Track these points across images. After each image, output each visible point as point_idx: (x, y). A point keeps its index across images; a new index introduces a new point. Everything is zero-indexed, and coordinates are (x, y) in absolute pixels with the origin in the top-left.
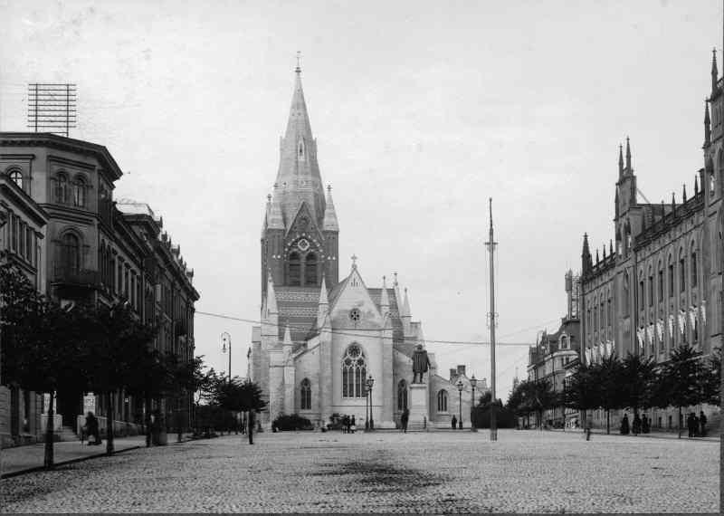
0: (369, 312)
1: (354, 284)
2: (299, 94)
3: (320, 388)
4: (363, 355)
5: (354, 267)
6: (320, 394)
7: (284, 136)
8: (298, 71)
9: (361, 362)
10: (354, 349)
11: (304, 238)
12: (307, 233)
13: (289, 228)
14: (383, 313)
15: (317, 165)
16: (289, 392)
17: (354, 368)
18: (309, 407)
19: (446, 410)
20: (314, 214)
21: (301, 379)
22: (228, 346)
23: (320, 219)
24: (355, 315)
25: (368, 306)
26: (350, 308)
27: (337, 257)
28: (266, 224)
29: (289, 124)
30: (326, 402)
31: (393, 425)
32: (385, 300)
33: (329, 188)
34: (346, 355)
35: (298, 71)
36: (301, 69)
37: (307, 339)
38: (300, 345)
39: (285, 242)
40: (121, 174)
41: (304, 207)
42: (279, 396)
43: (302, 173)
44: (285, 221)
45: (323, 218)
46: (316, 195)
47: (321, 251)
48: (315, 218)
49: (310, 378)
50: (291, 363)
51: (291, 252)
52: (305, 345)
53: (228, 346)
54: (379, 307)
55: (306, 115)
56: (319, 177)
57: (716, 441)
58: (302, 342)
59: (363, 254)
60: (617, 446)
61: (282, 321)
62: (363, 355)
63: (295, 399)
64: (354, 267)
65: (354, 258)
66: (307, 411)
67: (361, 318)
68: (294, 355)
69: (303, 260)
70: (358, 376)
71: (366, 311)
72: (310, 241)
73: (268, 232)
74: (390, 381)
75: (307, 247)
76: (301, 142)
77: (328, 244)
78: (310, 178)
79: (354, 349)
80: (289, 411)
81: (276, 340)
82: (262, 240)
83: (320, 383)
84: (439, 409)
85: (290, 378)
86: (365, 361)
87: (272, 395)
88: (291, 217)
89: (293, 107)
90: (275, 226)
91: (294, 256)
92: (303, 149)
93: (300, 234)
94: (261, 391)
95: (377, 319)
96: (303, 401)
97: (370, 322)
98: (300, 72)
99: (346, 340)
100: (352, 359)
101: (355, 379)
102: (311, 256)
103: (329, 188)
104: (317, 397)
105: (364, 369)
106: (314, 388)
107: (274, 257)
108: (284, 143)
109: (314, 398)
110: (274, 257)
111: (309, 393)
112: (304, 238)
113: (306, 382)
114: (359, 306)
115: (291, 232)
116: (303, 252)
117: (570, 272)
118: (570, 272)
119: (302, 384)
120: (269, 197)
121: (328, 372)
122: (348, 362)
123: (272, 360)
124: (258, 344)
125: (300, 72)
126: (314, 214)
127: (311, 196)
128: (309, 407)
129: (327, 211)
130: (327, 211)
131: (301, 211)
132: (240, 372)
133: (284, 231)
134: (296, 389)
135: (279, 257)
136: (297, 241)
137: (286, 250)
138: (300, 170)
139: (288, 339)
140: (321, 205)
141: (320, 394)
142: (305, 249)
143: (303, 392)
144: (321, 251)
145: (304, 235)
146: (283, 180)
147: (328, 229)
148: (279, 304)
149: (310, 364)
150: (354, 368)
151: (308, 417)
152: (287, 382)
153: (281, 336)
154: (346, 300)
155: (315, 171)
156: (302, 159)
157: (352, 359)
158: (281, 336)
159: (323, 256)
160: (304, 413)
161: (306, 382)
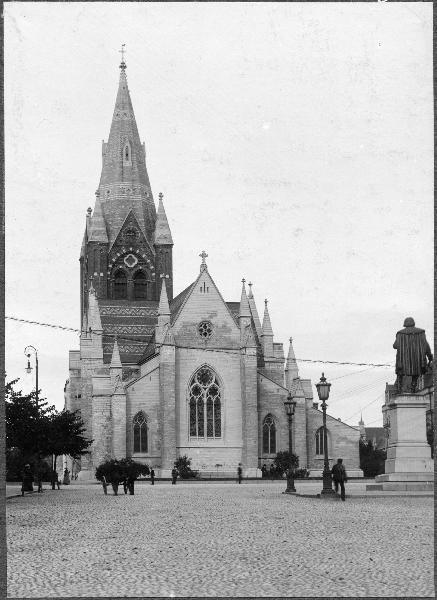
0: (224, 326)
1: (204, 289)
2: (124, 91)
3: (161, 424)
4: (216, 382)
5: (204, 268)
6: (160, 432)
7: (106, 141)
8: (123, 66)
9: (213, 391)
10: (204, 375)
11: (130, 252)
12: (135, 247)
13: (113, 241)
14: (243, 327)
15: (146, 171)
16: (120, 430)
17: (205, 400)
18: (145, 449)
20: (143, 226)
21: (134, 412)
22: (33, 365)
23: (151, 231)
24: (205, 329)
25: (223, 318)
26: (199, 320)
27: (171, 274)
28: (86, 238)
29: (113, 127)
30: (168, 444)
31: (361, 473)
32: (244, 312)
33: (161, 196)
34: (193, 382)
35: (123, 66)
36: (126, 64)
37: (140, 363)
38: (132, 371)
41: (131, 218)
42: (106, 436)
43: (128, 180)
44: (108, 233)
45: (154, 230)
46: (146, 211)
48: (143, 230)
49: (93, 472)
50: (121, 391)
51: (116, 269)
52: (137, 371)
53: (33, 365)
54: (238, 321)
55: (132, 116)
56: (149, 185)
57: (428, 496)
58: (136, 367)
59: (204, 246)
60: (207, 489)
61: (107, 339)
62: (216, 382)
63: (127, 440)
64: (204, 268)
65: (204, 255)
66: (141, 455)
67: (214, 331)
68: (124, 383)
69: (130, 281)
70: (209, 409)
71: (220, 325)
72: (139, 256)
73: (89, 245)
74: (253, 415)
75: (134, 264)
76: (128, 144)
77: (157, 259)
78: (138, 186)
79: (204, 375)
80: (119, 455)
81: (100, 364)
82: (81, 260)
83: (160, 417)
86: (220, 390)
87: (94, 428)
88: (116, 229)
89: (117, 106)
90: (97, 238)
91: (120, 274)
92: (130, 152)
93: (127, 247)
94: (80, 425)
95: (235, 334)
96: (137, 440)
97: (225, 339)
98: (125, 67)
99: (195, 360)
100: (201, 386)
102: (140, 274)
103: (161, 196)
105: (218, 400)
106: (153, 425)
107: (96, 274)
108: (107, 149)
109: (153, 440)
110: (96, 274)
111: (145, 430)
112: (130, 252)
113: (141, 416)
114: (211, 317)
115: (115, 245)
117: (409, 323)
118: (409, 323)
119: (135, 419)
120: (90, 210)
121: (170, 405)
122: (196, 391)
124: (75, 371)
125: (125, 67)
126: (143, 226)
127: (139, 206)
128: (145, 449)
129: (158, 223)
130: (158, 222)
131: (127, 222)
132: (54, 400)
133: (108, 245)
134: (128, 426)
135: (102, 274)
136: (123, 256)
137: (110, 266)
138: (125, 176)
139: (116, 359)
140: (152, 218)
141: (160, 432)
143: (136, 431)
148: (105, 320)
149: (146, 392)
150: (205, 400)
151: (143, 462)
152: (116, 416)
153: (107, 359)
154: (191, 314)
155: (144, 179)
156: (127, 164)
157: (201, 386)
158: (107, 359)
160: (139, 458)
161: (141, 416)
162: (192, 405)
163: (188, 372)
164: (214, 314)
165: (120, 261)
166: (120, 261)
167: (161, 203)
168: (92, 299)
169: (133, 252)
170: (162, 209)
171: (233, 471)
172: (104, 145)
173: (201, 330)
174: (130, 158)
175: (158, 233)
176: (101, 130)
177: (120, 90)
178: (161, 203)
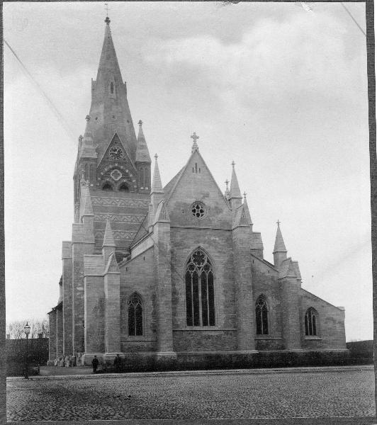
0: (216, 208)
4: (208, 261)
6: (155, 314)
7: (95, 79)
8: (107, 21)
10: (199, 256)
16: (113, 313)
18: (140, 333)
19: (315, 334)
21: (305, 308)
33: (140, 123)
34: (190, 261)
35: (107, 21)
39: (98, 170)
40: (64, 243)
47: (134, 181)
51: (103, 181)
64: (196, 151)
65: (195, 137)
71: (213, 206)
72: (122, 171)
73: (83, 161)
79: (199, 256)
84: (307, 334)
85: (112, 294)
101: (200, 295)
103: (140, 123)
104: (150, 318)
106: (147, 306)
108: (95, 86)
109: (147, 319)
115: (103, 161)
116: (116, 182)
121: (167, 284)
122: (192, 267)
123: (86, 266)
133: (96, 160)
142: (117, 179)
143: (131, 311)
144: (134, 181)
145: (116, 165)
146: (96, 111)
147: (140, 160)
159: (135, 187)
161: (136, 298)
162: (188, 277)
163: (188, 252)
164: (207, 195)
165: (107, 174)
166: (107, 174)
167: (141, 130)
168: (85, 191)
169: (119, 169)
170: (142, 139)
171: (280, 333)
172: (93, 82)
173: (194, 211)
174: (114, 91)
175: (139, 151)
176: (91, 73)
177: (105, 39)
178: (141, 130)
